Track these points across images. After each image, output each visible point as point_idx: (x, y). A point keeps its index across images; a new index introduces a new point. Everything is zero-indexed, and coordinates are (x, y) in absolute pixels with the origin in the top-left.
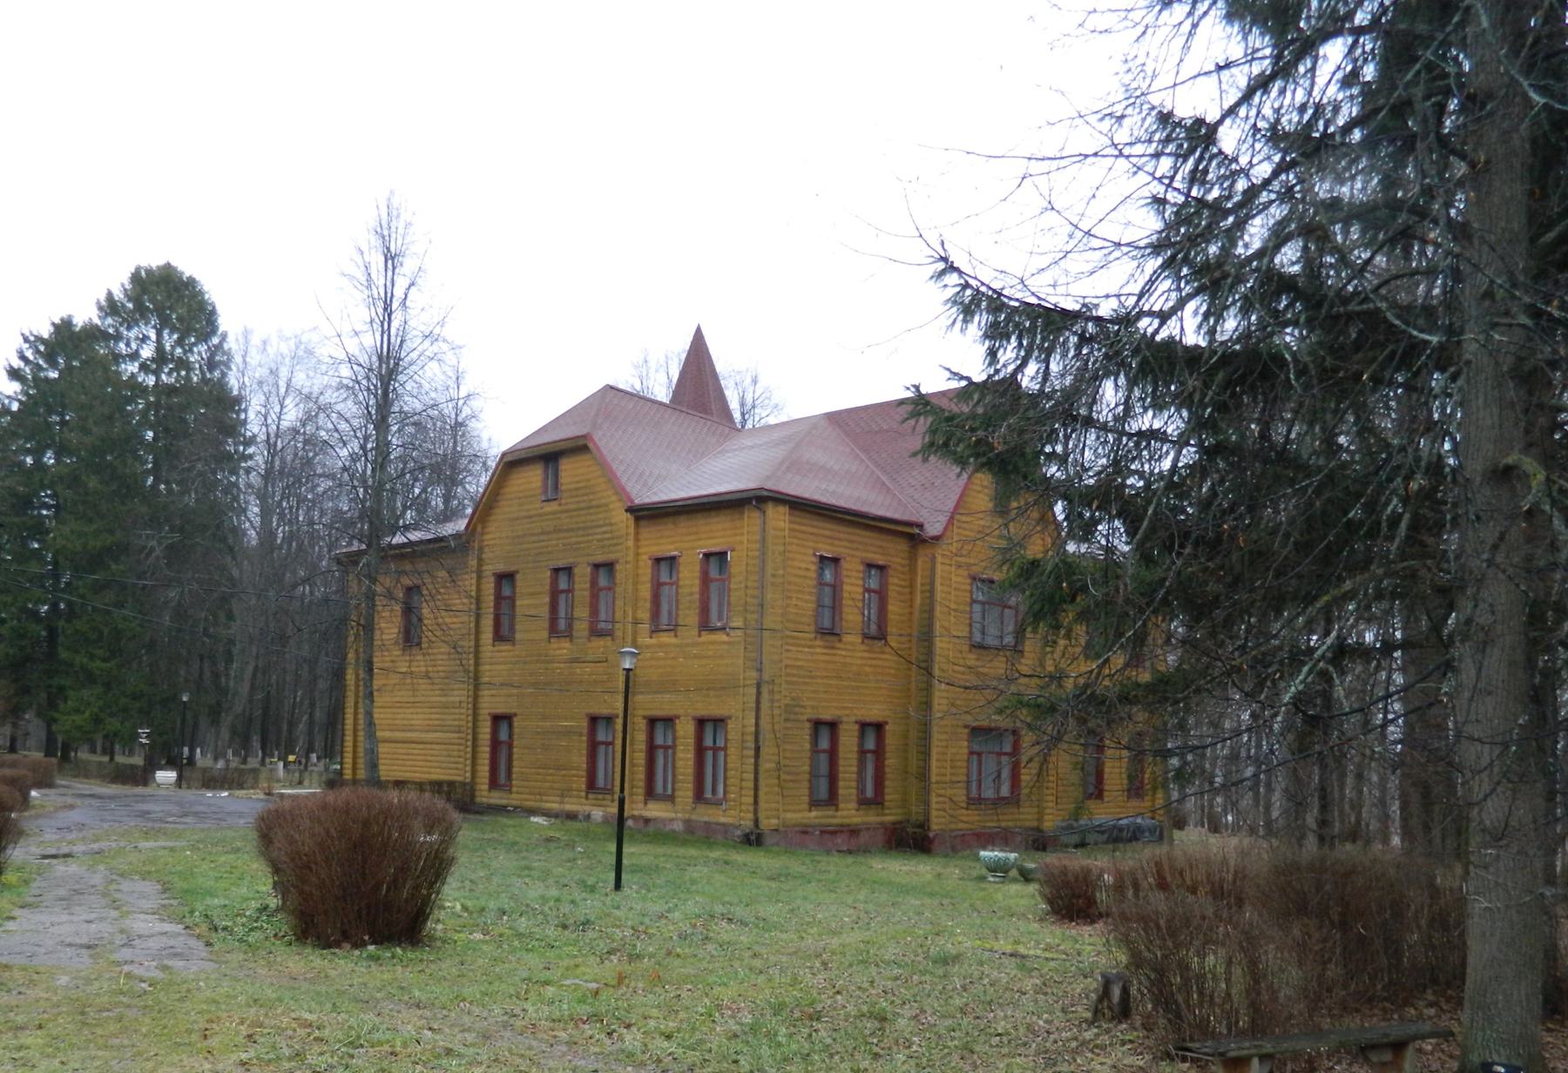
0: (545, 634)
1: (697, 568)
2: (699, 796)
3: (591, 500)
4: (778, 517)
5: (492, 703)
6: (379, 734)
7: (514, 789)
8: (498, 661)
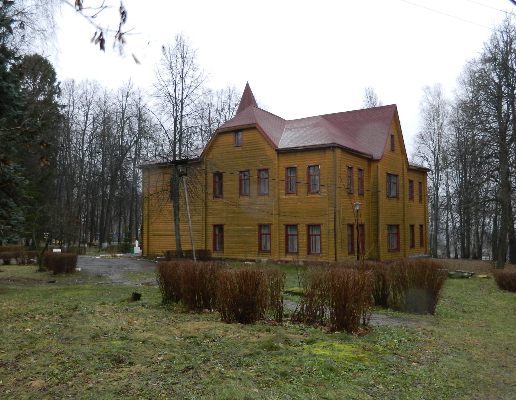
0: (238, 195)
1: (306, 171)
2: (309, 252)
3: (256, 147)
4: (338, 152)
5: (213, 220)
6: (181, 233)
7: (225, 252)
8: (215, 205)
